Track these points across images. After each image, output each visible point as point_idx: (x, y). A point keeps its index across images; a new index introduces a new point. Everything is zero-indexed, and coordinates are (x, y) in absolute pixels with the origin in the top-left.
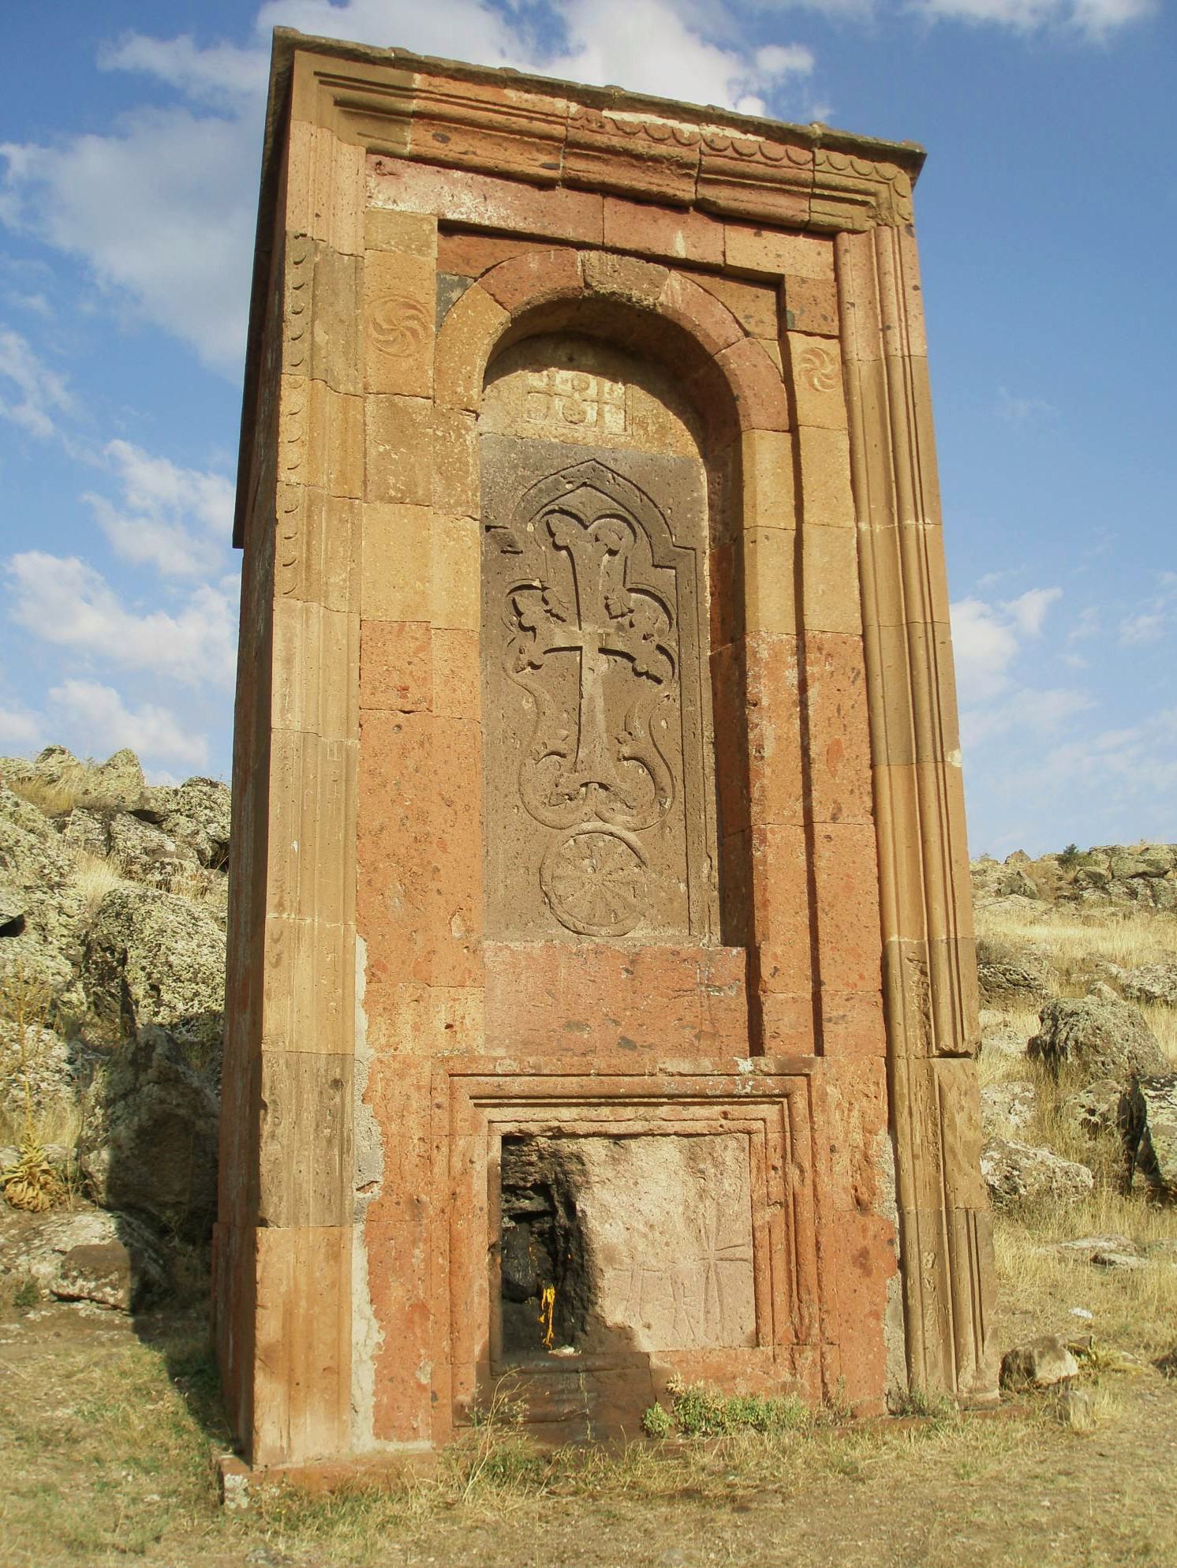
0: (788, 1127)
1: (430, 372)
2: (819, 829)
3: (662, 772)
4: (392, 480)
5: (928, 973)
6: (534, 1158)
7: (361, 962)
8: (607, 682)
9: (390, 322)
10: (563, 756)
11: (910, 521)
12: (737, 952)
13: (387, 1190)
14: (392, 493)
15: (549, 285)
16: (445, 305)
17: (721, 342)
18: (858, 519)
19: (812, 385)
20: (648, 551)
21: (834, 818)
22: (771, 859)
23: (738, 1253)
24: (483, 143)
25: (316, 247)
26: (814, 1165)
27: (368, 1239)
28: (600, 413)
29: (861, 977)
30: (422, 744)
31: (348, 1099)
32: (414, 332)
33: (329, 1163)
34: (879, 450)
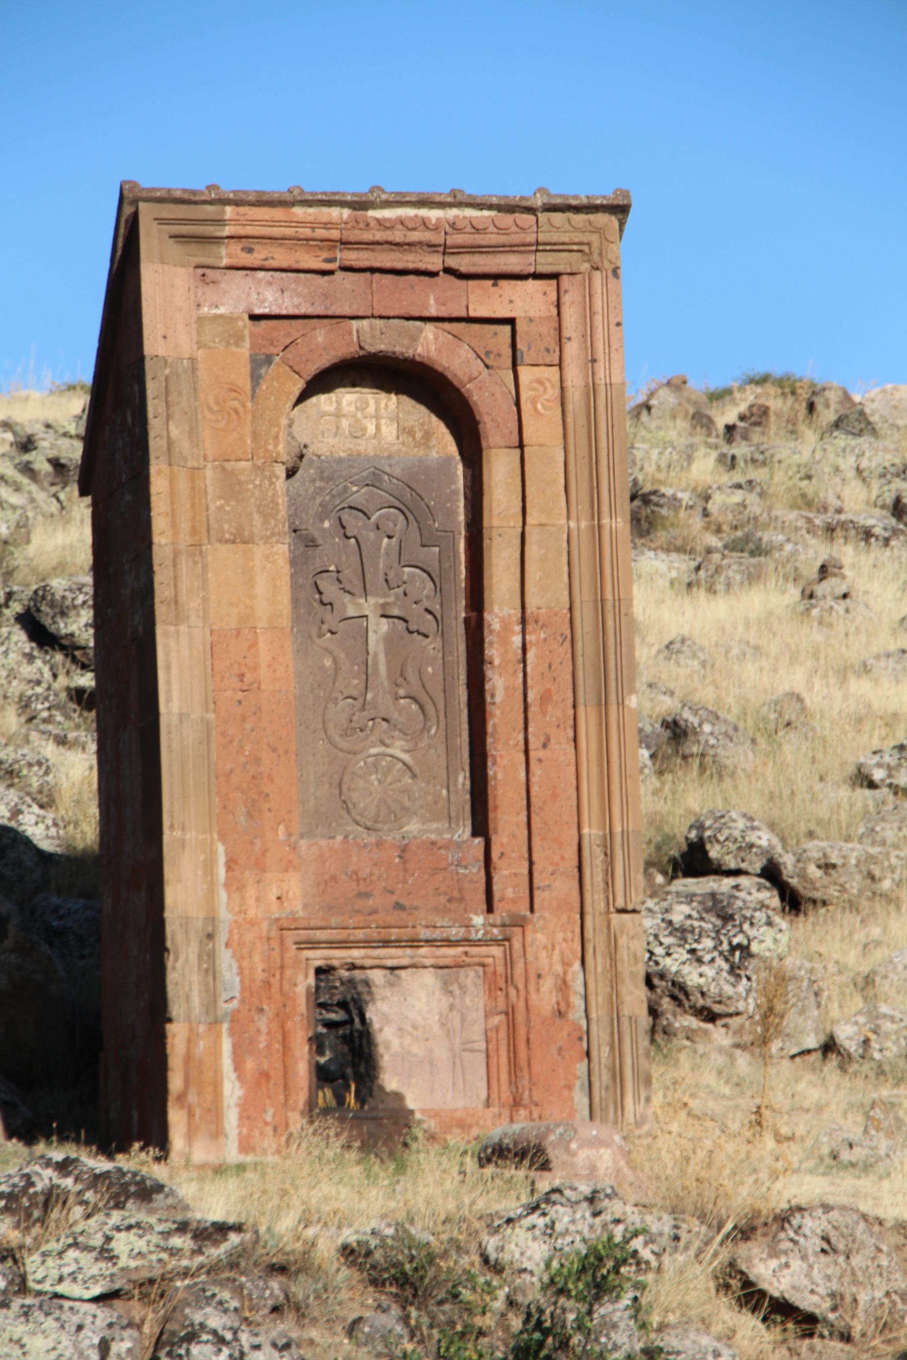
0: (509, 961)
1: (249, 442)
2: (532, 754)
3: (429, 707)
4: (226, 527)
5: (609, 857)
6: (338, 984)
7: (222, 860)
8: (389, 640)
9: (218, 403)
10: (355, 699)
11: (606, 521)
12: (479, 841)
13: (242, 1001)
14: (227, 536)
15: (333, 353)
16: (256, 379)
17: (466, 379)
18: (568, 518)
19: (536, 409)
20: (418, 533)
21: (545, 746)
22: (500, 776)
23: (475, 1046)
24: (280, 250)
25: (166, 362)
26: (526, 987)
27: (232, 1032)
28: (375, 424)
29: (563, 858)
30: (255, 713)
31: (217, 945)
32: (236, 411)
33: (207, 985)
34: (586, 461)
